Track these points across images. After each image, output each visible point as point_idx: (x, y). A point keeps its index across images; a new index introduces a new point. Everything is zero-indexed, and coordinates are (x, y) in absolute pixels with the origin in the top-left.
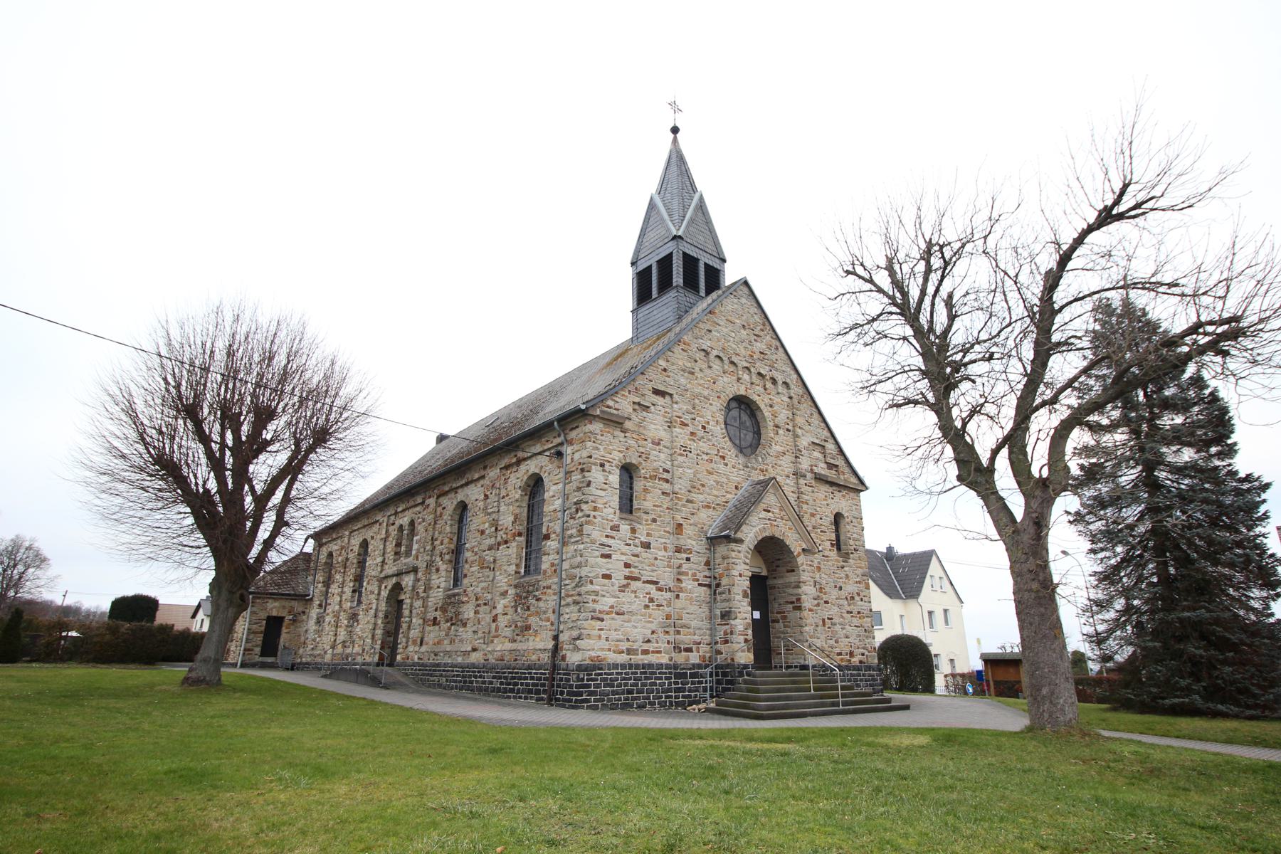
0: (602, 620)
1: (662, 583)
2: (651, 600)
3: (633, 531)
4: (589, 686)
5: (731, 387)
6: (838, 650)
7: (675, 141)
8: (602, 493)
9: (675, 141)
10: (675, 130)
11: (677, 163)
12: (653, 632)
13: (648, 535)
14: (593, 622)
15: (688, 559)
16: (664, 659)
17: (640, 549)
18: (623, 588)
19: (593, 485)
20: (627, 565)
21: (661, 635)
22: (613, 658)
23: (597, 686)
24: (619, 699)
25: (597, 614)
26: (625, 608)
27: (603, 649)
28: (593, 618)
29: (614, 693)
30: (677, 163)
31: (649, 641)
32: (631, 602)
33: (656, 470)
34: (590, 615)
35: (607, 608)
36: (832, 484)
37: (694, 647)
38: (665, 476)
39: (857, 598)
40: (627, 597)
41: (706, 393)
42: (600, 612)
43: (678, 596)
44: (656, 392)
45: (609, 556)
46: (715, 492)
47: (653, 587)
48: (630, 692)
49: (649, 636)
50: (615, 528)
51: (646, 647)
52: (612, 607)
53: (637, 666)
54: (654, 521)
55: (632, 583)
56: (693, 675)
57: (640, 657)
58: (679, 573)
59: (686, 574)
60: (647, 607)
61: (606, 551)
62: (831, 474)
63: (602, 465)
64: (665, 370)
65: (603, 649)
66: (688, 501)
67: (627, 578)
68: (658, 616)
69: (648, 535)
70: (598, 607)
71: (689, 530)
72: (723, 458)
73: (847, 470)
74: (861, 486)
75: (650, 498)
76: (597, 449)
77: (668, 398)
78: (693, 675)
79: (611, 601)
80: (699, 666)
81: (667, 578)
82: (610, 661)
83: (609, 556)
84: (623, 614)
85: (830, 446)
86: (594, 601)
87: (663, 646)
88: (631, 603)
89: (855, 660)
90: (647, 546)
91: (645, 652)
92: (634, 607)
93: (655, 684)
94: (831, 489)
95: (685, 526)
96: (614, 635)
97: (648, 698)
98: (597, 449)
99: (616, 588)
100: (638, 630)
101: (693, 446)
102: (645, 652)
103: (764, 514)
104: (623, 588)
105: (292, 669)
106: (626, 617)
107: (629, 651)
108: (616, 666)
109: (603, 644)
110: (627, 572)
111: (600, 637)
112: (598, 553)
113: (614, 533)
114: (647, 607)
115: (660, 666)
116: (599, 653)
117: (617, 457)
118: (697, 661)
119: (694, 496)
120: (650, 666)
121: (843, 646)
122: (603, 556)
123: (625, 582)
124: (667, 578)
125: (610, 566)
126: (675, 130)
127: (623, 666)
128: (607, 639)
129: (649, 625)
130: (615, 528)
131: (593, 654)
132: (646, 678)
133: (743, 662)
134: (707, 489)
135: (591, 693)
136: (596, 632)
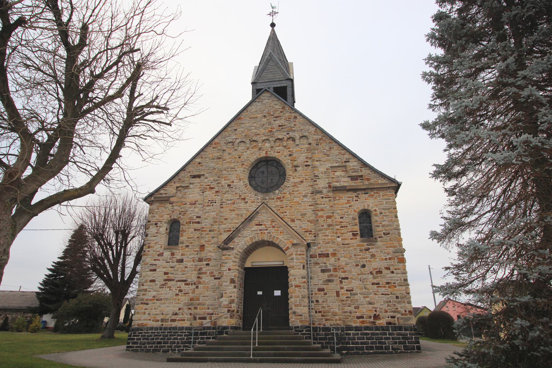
0: (147, 304)
1: (189, 280)
2: (180, 291)
3: (173, 254)
4: (134, 339)
5: (252, 155)
6: (358, 314)
7: (273, 31)
8: (154, 238)
9: (273, 31)
10: (273, 25)
11: (273, 42)
12: (180, 309)
13: (182, 255)
14: (141, 306)
15: (208, 265)
16: (187, 324)
17: (175, 264)
18: (162, 286)
19: (149, 235)
20: (166, 273)
21: (186, 311)
22: (151, 324)
23: (139, 339)
24: (152, 347)
25: (145, 301)
26: (162, 297)
27: (146, 320)
28: (141, 303)
29: (148, 343)
30: (273, 42)
31: (176, 314)
32: (165, 293)
33: (192, 218)
34: (140, 302)
35: (151, 298)
36: (355, 190)
37: (208, 316)
38: (198, 220)
39: (385, 272)
40: (165, 290)
41: (232, 165)
42: (146, 300)
43: (197, 287)
44: (194, 177)
45: (155, 270)
46: (236, 221)
47: (183, 283)
48: (160, 343)
49: (178, 311)
50: (161, 255)
51: (174, 317)
52: (154, 297)
53: (166, 329)
54: (187, 246)
55: (169, 282)
56: (202, 334)
57: (170, 323)
58: (199, 274)
59: (206, 273)
60: (177, 295)
61: (153, 267)
62: (358, 184)
63: (156, 224)
64: (199, 163)
65: (146, 320)
66: (210, 231)
67: (165, 280)
68: (184, 299)
69: (182, 255)
70: (145, 297)
71: (208, 248)
72: (244, 199)
73: (373, 175)
74: (396, 186)
75: (187, 234)
76: (154, 217)
77: (202, 177)
78: (202, 334)
79: (154, 293)
80: (208, 328)
81: (192, 277)
82: (149, 326)
83: (155, 270)
84: (161, 300)
85: (353, 164)
86: (143, 294)
87: (187, 316)
88: (166, 294)
89: (382, 322)
90: (181, 261)
91: (174, 320)
92: (168, 296)
93: (177, 339)
94: (355, 194)
95: (206, 245)
96: (153, 312)
97: (171, 347)
98: (154, 217)
99: (158, 286)
100: (169, 309)
101: (218, 199)
102: (174, 320)
103: (256, 228)
104: (162, 286)
105: (35, 332)
106: (163, 301)
107: (162, 320)
108: (152, 328)
109: (146, 316)
110: (165, 277)
111: (145, 313)
112: (147, 270)
113: (160, 258)
114: (177, 295)
115: (182, 328)
116: (144, 322)
117: (166, 217)
118: (209, 325)
119: (216, 227)
120: (175, 328)
121: (365, 310)
122: (151, 270)
123: (164, 282)
124: (192, 277)
125: (155, 275)
126: (273, 25)
127: (156, 329)
128: (149, 314)
129: (178, 305)
130: (161, 255)
131: (140, 322)
132: (170, 335)
133: (224, 325)
134: (229, 221)
135: (134, 343)
136: (143, 311)
